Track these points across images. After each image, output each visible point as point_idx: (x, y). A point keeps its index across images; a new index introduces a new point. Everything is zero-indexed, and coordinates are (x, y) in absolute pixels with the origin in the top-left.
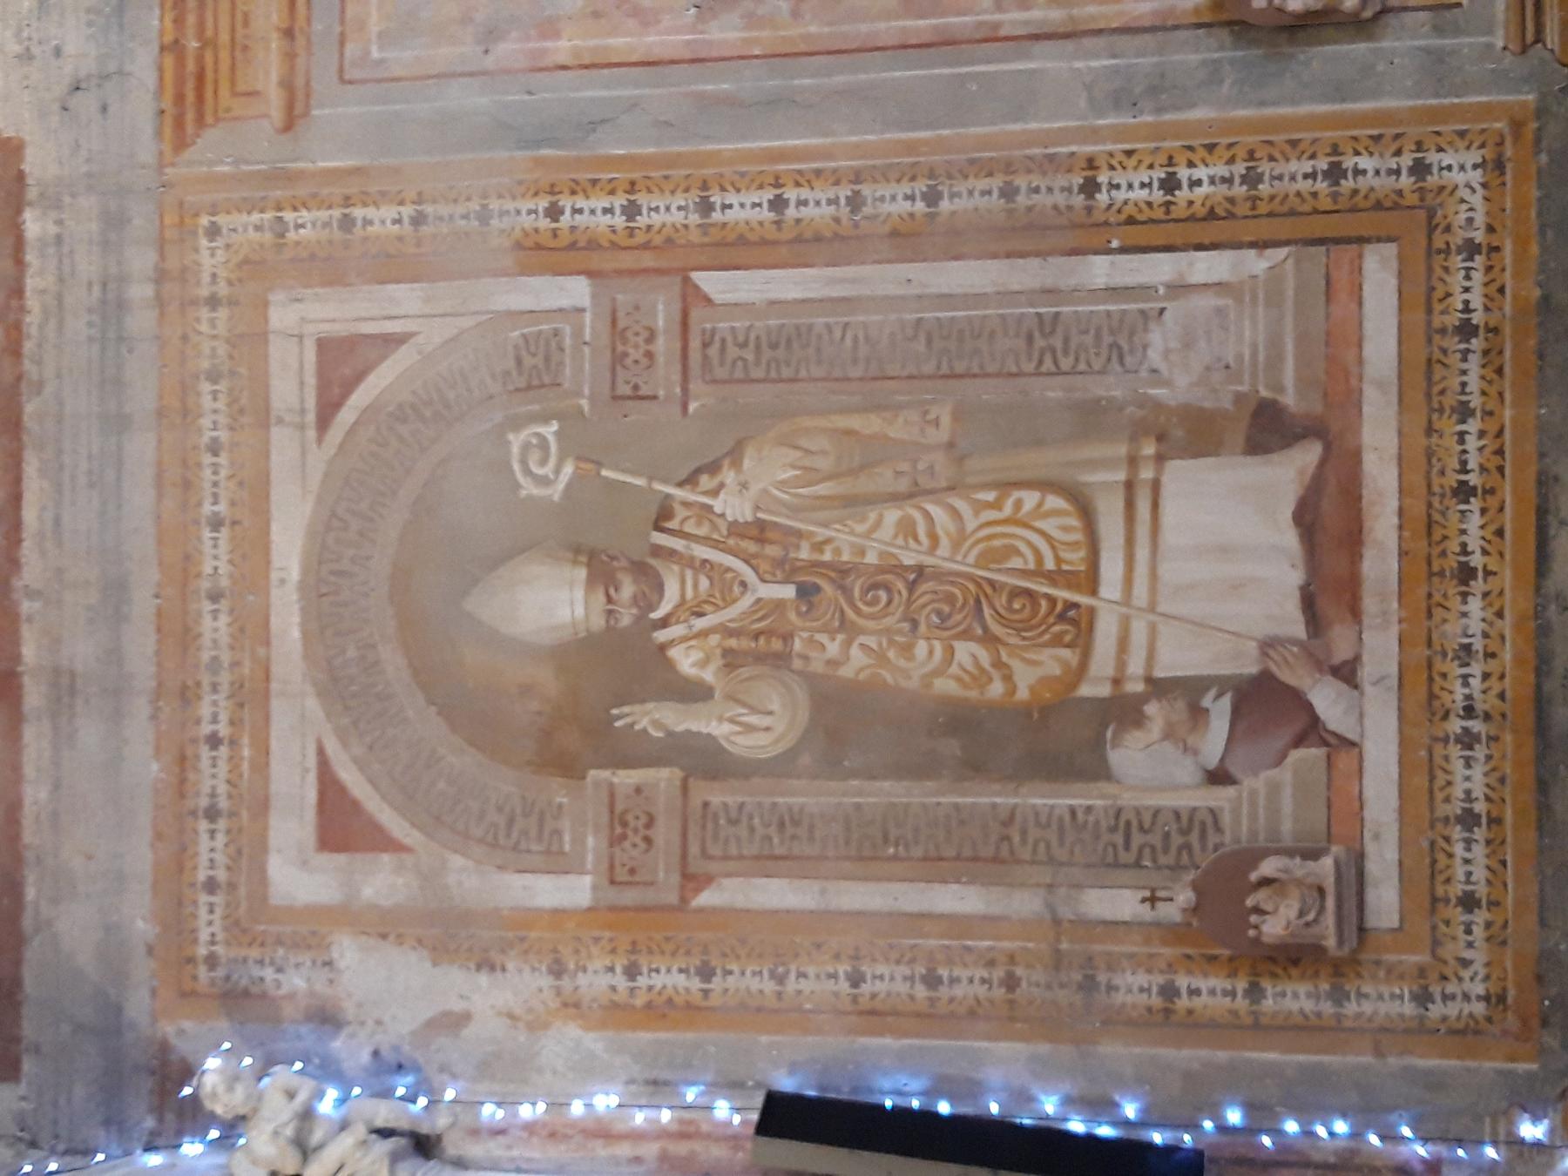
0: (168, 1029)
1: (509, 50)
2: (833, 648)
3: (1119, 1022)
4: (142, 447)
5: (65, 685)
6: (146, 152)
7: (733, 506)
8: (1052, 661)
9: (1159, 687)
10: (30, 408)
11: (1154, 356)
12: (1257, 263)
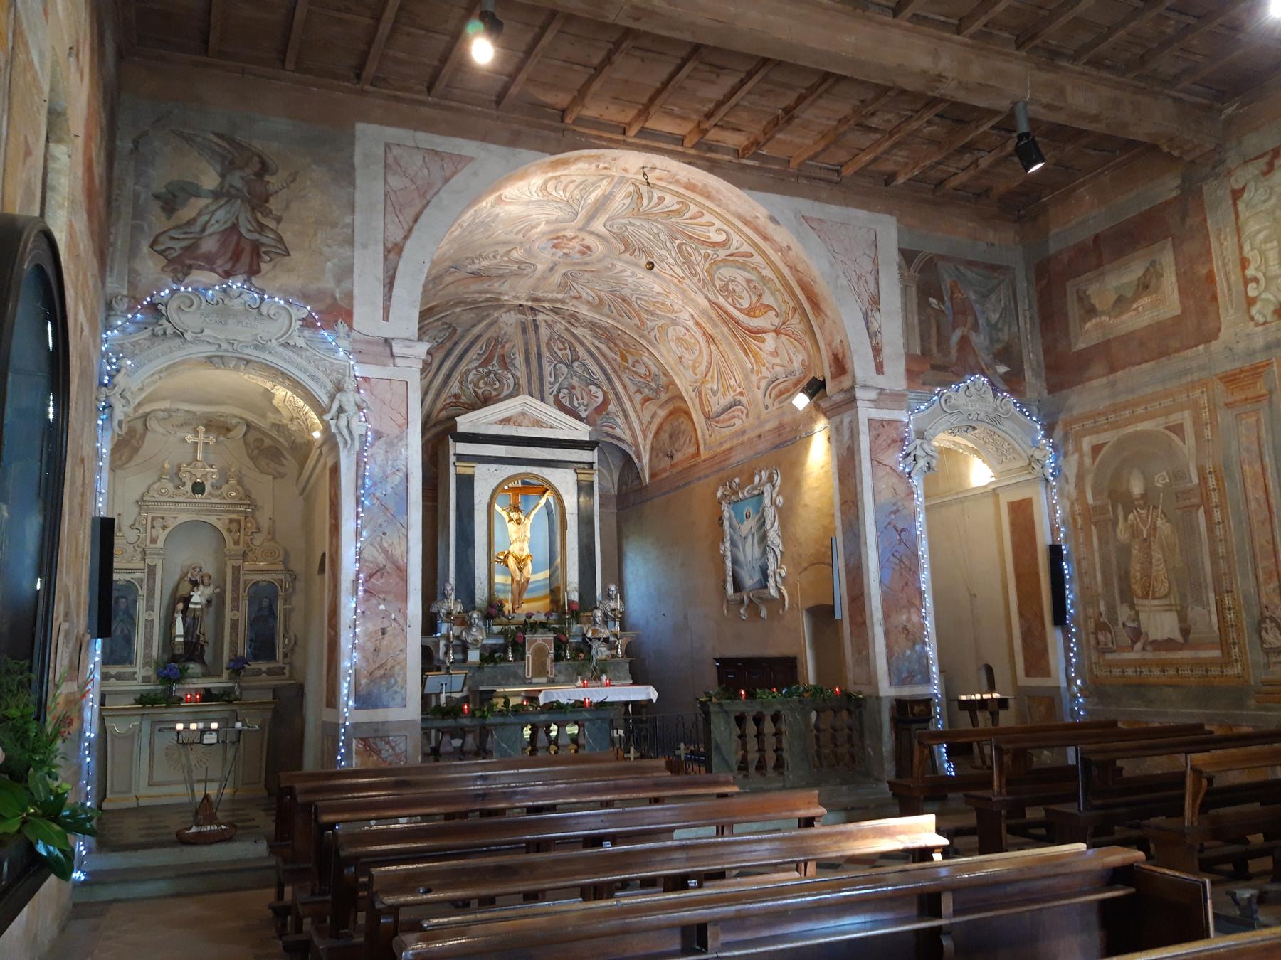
0: (1060, 422)
1: (1244, 454)
2: (1137, 547)
3: (1085, 609)
4: (1159, 388)
5: (1113, 384)
6: (1219, 371)
7: (1159, 522)
8: (1139, 591)
9: (1137, 613)
10: (1164, 359)
11: (1196, 608)
12: (1216, 628)
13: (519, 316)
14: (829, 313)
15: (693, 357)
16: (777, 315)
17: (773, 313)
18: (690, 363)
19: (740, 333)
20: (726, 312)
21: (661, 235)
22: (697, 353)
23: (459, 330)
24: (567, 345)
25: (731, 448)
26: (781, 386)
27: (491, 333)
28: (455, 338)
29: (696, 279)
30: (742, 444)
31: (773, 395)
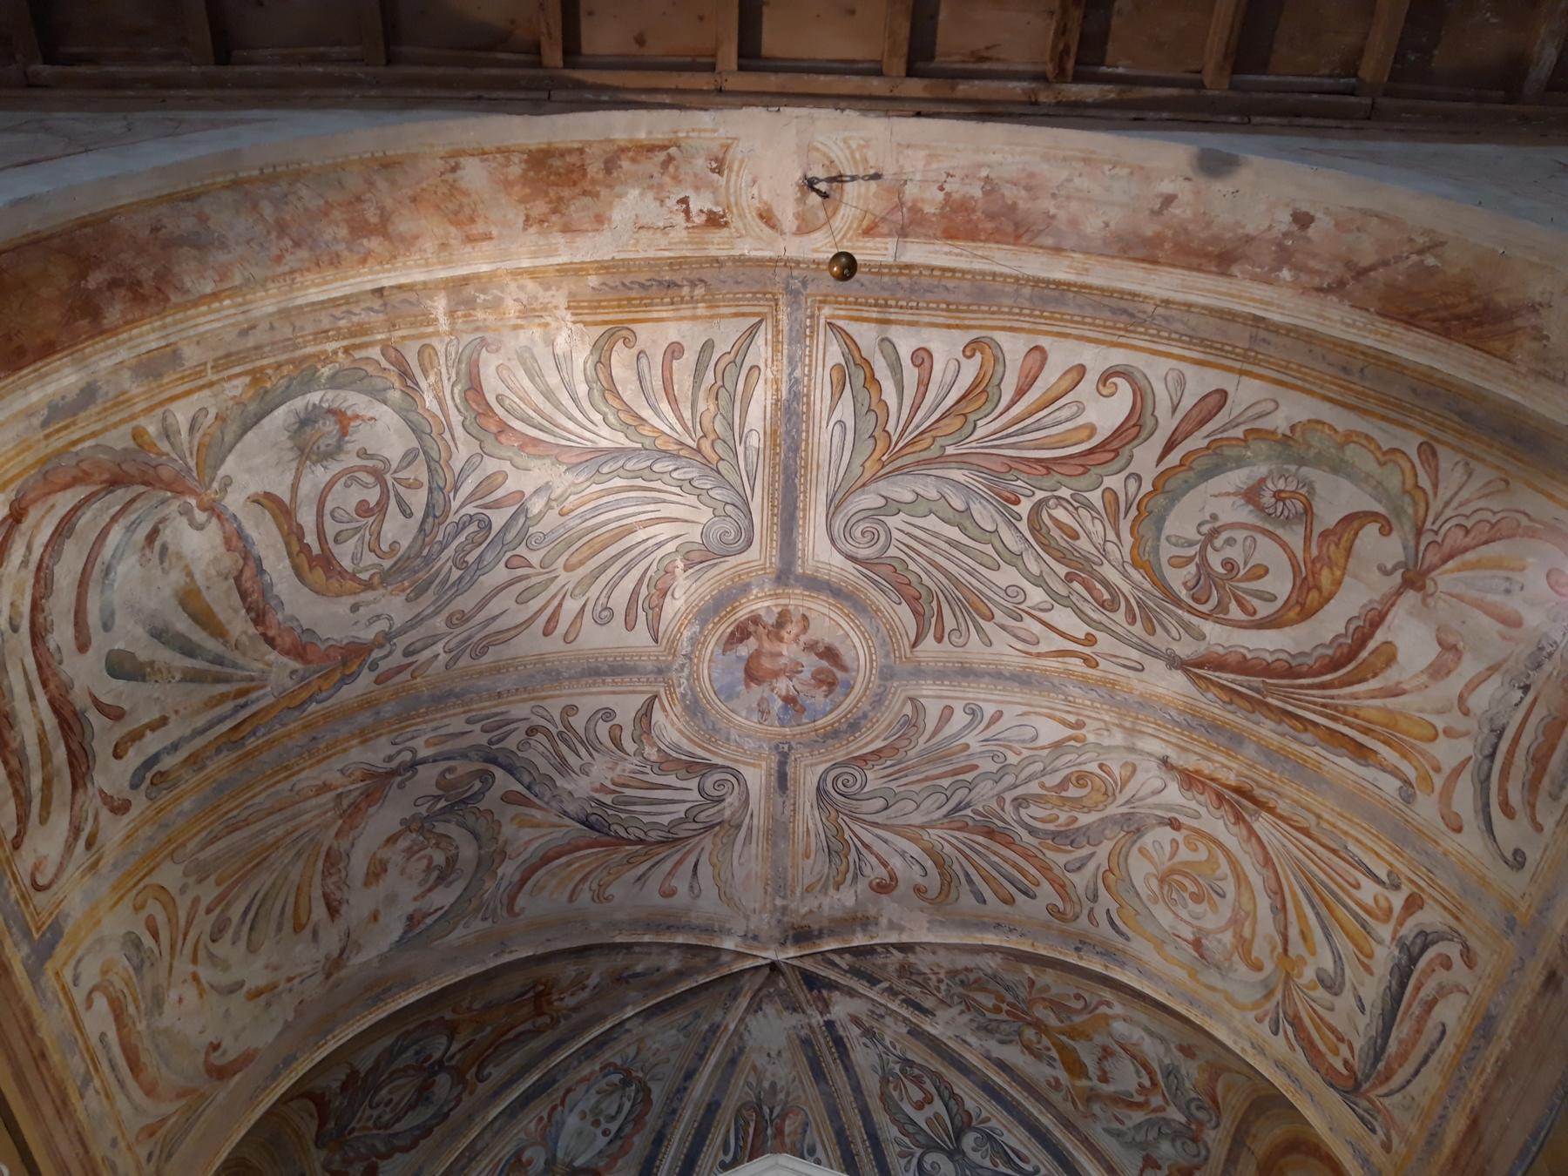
13: (792, 1020)
14: (1537, 289)
15: (1226, 912)
16: (1387, 529)
17: (1372, 529)
18: (1228, 938)
19: (1309, 702)
20: (1244, 666)
21: (976, 508)
22: (1229, 887)
23: (657, 1092)
24: (929, 1085)
25: (1474, 1123)
26: (1525, 741)
27: (738, 1093)
28: (652, 1120)
29: (1120, 617)
30: (1503, 1070)
31: (1515, 798)
